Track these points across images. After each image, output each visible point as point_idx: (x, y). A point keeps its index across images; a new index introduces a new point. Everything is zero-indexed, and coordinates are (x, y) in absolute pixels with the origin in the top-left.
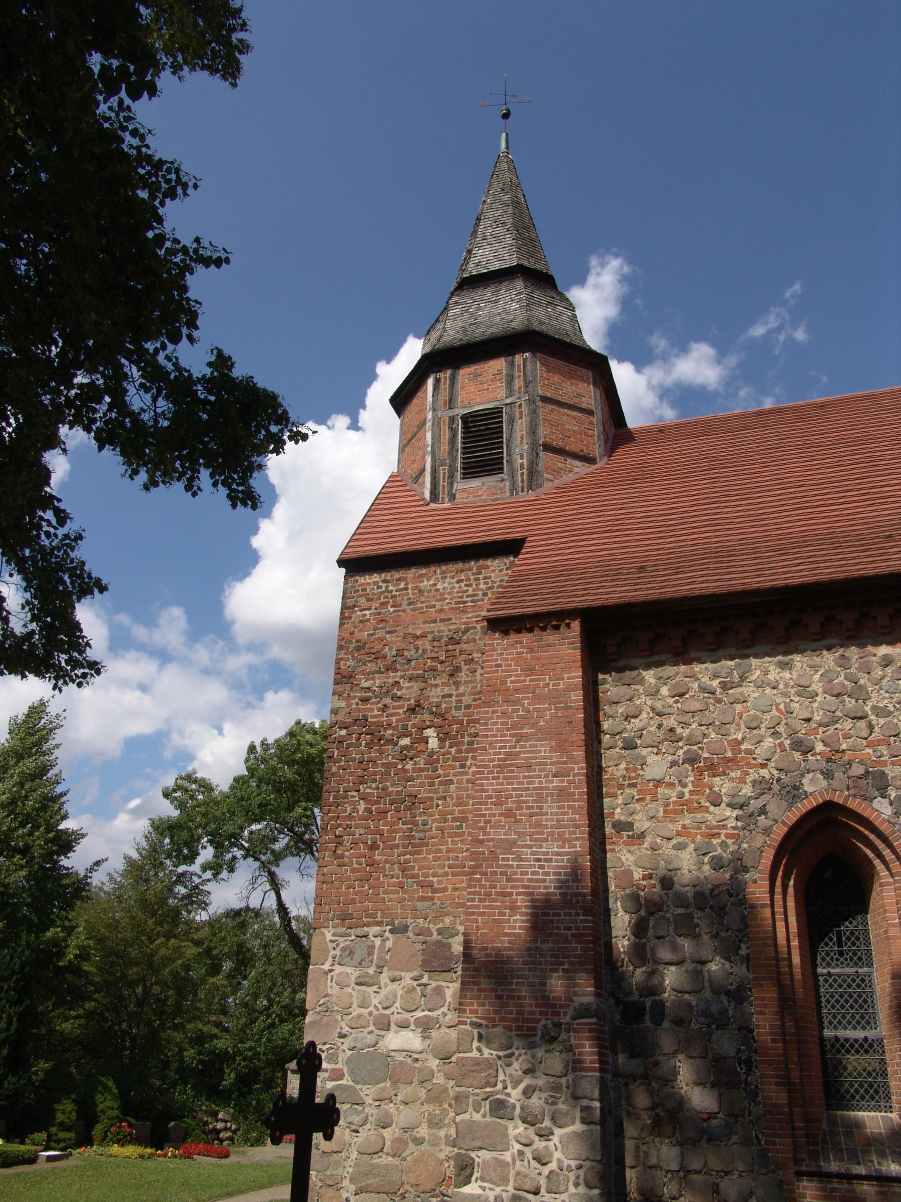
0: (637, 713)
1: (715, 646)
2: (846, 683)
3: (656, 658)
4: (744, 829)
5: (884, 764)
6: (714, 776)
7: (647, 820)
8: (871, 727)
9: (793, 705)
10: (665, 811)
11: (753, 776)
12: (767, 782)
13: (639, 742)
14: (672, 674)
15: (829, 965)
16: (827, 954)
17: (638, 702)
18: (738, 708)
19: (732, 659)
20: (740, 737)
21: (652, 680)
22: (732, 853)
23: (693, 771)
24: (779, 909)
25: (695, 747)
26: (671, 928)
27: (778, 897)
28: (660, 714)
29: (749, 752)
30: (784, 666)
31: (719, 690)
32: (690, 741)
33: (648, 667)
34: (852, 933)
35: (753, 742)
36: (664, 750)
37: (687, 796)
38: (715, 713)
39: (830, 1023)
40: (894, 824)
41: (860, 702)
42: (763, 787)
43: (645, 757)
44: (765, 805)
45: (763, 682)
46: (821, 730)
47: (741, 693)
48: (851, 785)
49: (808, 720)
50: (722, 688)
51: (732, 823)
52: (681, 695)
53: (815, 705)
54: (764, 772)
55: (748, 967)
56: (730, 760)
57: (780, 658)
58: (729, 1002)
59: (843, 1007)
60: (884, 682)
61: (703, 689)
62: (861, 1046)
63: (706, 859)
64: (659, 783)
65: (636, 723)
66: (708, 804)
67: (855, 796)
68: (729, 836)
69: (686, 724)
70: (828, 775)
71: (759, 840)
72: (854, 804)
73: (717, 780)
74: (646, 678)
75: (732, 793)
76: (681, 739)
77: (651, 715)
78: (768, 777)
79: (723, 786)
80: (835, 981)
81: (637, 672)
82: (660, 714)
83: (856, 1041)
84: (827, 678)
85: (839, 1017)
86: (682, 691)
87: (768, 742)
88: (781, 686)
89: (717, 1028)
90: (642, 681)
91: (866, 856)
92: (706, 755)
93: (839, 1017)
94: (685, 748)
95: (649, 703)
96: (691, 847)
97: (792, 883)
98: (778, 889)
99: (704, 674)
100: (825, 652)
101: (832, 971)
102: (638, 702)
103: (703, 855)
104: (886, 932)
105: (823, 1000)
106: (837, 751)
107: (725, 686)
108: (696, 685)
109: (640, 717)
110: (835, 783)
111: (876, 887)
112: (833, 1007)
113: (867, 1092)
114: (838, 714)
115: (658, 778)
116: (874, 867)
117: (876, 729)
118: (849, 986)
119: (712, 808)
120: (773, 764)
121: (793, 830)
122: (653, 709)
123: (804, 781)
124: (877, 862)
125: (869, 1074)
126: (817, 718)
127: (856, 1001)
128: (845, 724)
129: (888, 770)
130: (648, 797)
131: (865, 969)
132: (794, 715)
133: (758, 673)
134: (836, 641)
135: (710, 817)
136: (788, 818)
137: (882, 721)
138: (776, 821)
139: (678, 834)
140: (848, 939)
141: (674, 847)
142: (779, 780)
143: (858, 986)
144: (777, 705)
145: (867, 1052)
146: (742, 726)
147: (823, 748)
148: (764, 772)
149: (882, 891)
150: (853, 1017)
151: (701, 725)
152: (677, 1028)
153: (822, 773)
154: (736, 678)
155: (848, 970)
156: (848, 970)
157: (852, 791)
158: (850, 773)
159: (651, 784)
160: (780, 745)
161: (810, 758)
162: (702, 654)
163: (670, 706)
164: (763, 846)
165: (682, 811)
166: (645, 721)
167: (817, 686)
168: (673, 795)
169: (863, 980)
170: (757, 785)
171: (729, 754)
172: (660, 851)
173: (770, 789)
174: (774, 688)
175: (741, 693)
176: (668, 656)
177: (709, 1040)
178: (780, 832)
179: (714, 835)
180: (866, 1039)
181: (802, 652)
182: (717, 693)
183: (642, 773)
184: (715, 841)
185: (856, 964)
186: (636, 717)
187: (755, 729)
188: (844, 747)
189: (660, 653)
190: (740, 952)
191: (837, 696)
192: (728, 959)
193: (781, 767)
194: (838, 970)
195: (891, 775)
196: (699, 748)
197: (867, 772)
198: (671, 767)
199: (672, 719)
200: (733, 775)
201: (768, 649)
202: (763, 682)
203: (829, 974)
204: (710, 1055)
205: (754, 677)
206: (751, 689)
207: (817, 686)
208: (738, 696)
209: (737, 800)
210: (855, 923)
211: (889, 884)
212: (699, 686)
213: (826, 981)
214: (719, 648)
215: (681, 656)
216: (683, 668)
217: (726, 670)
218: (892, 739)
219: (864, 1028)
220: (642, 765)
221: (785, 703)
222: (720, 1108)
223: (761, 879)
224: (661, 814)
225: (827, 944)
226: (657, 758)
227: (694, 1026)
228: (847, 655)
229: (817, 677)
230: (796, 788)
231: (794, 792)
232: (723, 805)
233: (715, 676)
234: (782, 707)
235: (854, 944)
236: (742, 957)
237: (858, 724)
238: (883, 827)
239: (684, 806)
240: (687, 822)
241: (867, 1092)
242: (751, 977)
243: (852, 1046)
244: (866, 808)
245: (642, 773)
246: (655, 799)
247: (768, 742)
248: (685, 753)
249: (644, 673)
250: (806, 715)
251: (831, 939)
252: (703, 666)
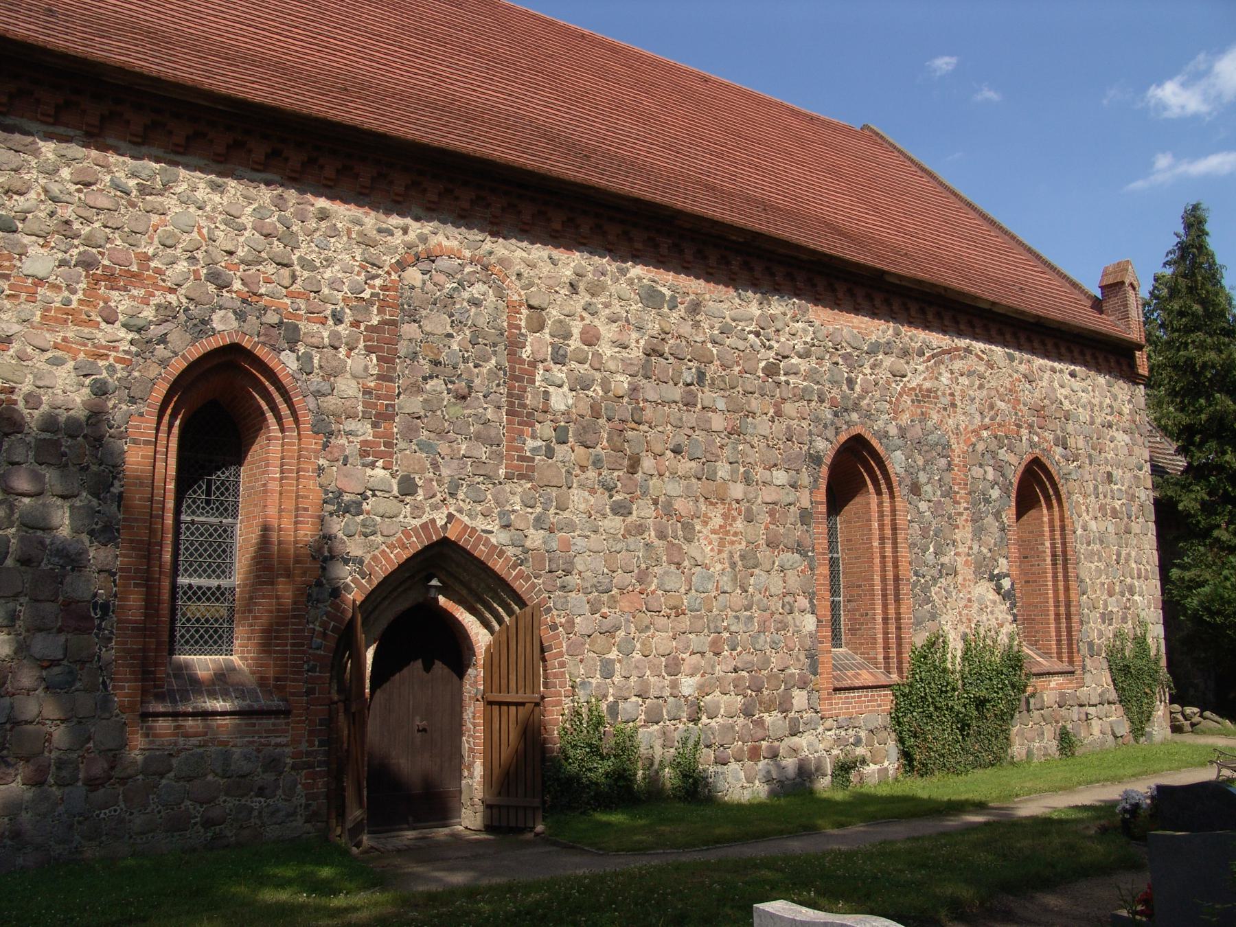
0: (24, 190)
1: (139, 140)
2: (278, 225)
3: (61, 130)
4: (138, 355)
5: (299, 318)
6: (112, 289)
7: (17, 322)
8: (294, 278)
9: (217, 232)
10: (43, 317)
11: (158, 298)
12: (173, 309)
13: (20, 226)
14: (80, 155)
15: (193, 513)
16: (194, 502)
17: (27, 177)
18: (155, 219)
19: (157, 162)
20: (151, 252)
21: (51, 156)
22: (119, 379)
23: (86, 277)
24: (161, 449)
25: (94, 250)
26: (31, 454)
27: (162, 435)
28: (54, 200)
29: (158, 271)
30: (215, 187)
31: (134, 193)
32: (88, 242)
33: (48, 137)
34: (223, 484)
35: (165, 261)
36: (53, 244)
37: (74, 305)
38: (126, 217)
39: (186, 570)
40: (297, 380)
41: (289, 249)
42: (168, 314)
43: (25, 246)
44: (166, 334)
45: (189, 197)
46: (242, 267)
47: (161, 204)
48: (263, 331)
49: (231, 253)
50: (139, 191)
51: (125, 346)
52: (87, 185)
53: (241, 239)
54: (172, 298)
55: (119, 507)
56: (134, 275)
57: (212, 177)
58: (91, 542)
59: (201, 555)
60: (316, 235)
61: (116, 186)
62: (213, 594)
63: (88, 381)
64: (40, 281)
65: (20, 202)
66: (99, 319)
67: (264, 344)
68: (118, 360)
69: (87, 221)
70: (240, 316)
71: (154, 371)
72: (261, 352)
73: (115, 294)
74: (43, 150)
75: (130, 312)
76: (77, 236)
77: (43, 197)
78: (175, 304)
79: (122, 303)
80: (207, 530)
81: (30, 139)
82: (54, 200)
83: (209, 589)
84: (259, 213)
85: (196, 565)
86: (89, 179)
87: (182, 266)
88: (208, 208)
89: (73, 570)
90: (36, 153)
91: (260, 407)
92: (106, 262)
93: (196, 565)
94: (82, 248)
95: (42, 181)
96: (71, 364)
97: (178, 423)
98: (164, 427)
99: (121, 168)
100: (263, 186)
101: (196, 519)
102: (27, 177)
103: (85, 376)
104: (265, 485)
105: (182, 547)
106: (255, 294)
107: (143, 190)
108: (108, 178)
109: (27, 196)
110: (246, 327)
111: (261, 440)
112: (191, 555)
113: (211, 637)
114: (263, 254)
115: (40, 275)
116: (265, 419)
117: (299, 281)
118: (211, 535)
119: (103, 325)
120: (183, 291)
121: (193, 366)
122: (46, 191)
123: (214, 317)
124: (269, 415)
125: (216, 620)
126: (241, 253)
127: (215, 551)
128: (269, 267)
129: (301, 325)
130: (23, 296)
131: (230, 520)
132: (217, 243)
133: (185, 186)
134: (277, 178)
135: (99, 335)
136: (190, 352)
137: (306, 274)
138: (176, 354)
139: (56, 347)
140: (218, 488)
141: (48, 361)
142: (187, 310)
143: (220, 536)
144: (200, 228)
145: (217, 599)
146: (156, 240)
147: (241, 287)
148: (172, 298)
149: (268, 445)
150: (200, 566)
151: (106, 227)
152: (23, 568)
153: (235, 312)
154: (159, 186)
155: (212, 520)
156: (212, 520)
157: (262, 339)
158: (264, 319)
159: (30, 281)
160: (196, 272)
161: (225, 294)
162: (123, 145)
163: (70, 194)
164: (159, 377)
165: (66, 321)
166: (34, 202)
167: (247, 220)
168: (57, 300)
169: (225, 531)
170: (161, 311)
171: (134, 268)
172: (30, 363)
173: (175, 317)
174: (200, 208)
175: (161, 204)
176: (78, 132)
177: (61, 583)
178: (178, 365)
179: (100, 356)
180: (219, 587)
181: (239, 178)
182: (133, 195)
183: (19, 264)
184: (101, 363)
185: (221, 515)
186: (21, 194)
187: (170, 247)
188: (262, 291)
189: (67, 125)
190: (112, 489)
191: (267, 236)
192: (96, 495)
193: (192, 296)
194: (202, 519)
195: (303, 330)
196: (99, 253)
197: (281, 322)
198: (59, 266)
199: (70, 210)
200: (135, 292)
201: (202, 163)
202: (189, 197)
203: (193, 522)
204: (61, 598)
205: (179, 190)
206: (173, 202)
207: (247, 220)
208: (157, 206)
209: (133, 322)
210: (227, 474)
211: (277, 438)
212: (112, 180)
213: (188, 528)
214: (143, 144)
215: (94, 137)
216: (94, 153)
217: (147, 172)
218: (312, 294)
219: (218, 577)
220: (20, 255)
221: (209, 229)
222: (65, 655)
223: (149, 413)
224: (37, 318)
225: (195, 492)
226: (42, 251)
227: (45, 566)
228: (285, 196)
229: (249, 210)
230: (204, 322)
231: (201, 327)
232: (118, 324)
233: (134, 175)
234: (205, 231)
235: (222, 494)
236: (113, 495)
237: (282, 271)
238: (286, 381)
239: (67, 315)
240: (70, 335)
241: (211, 637)
242: (121, 517)
243: (204, 594)
244: (272, 359)
245: (19, 264)
246: (32, 299)
247: (182, 266)
248: (80, 253)
249: (41, 144)
250: (229, 247)
251: (200, 487)
252: (121, 159)
